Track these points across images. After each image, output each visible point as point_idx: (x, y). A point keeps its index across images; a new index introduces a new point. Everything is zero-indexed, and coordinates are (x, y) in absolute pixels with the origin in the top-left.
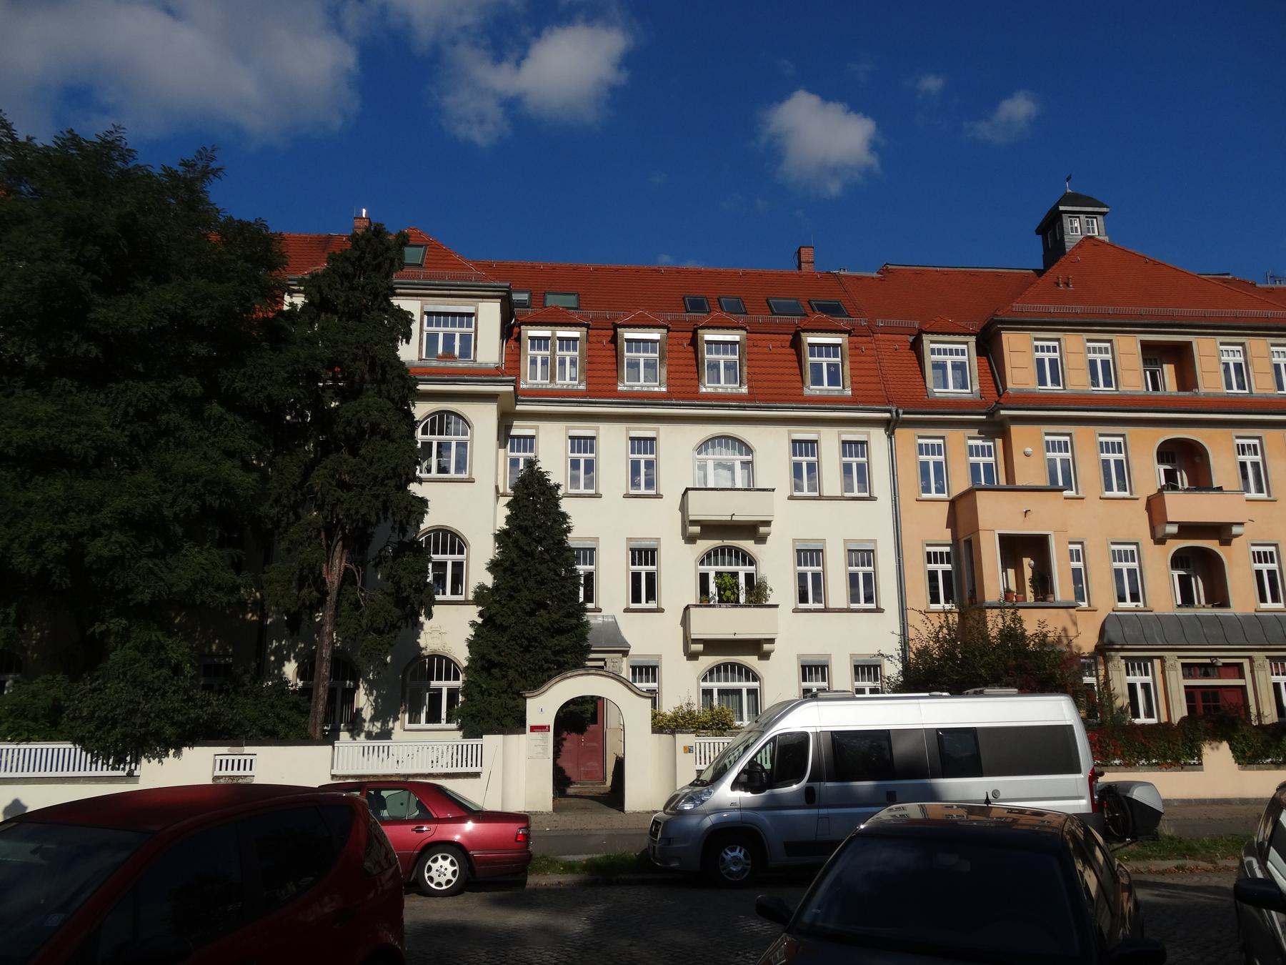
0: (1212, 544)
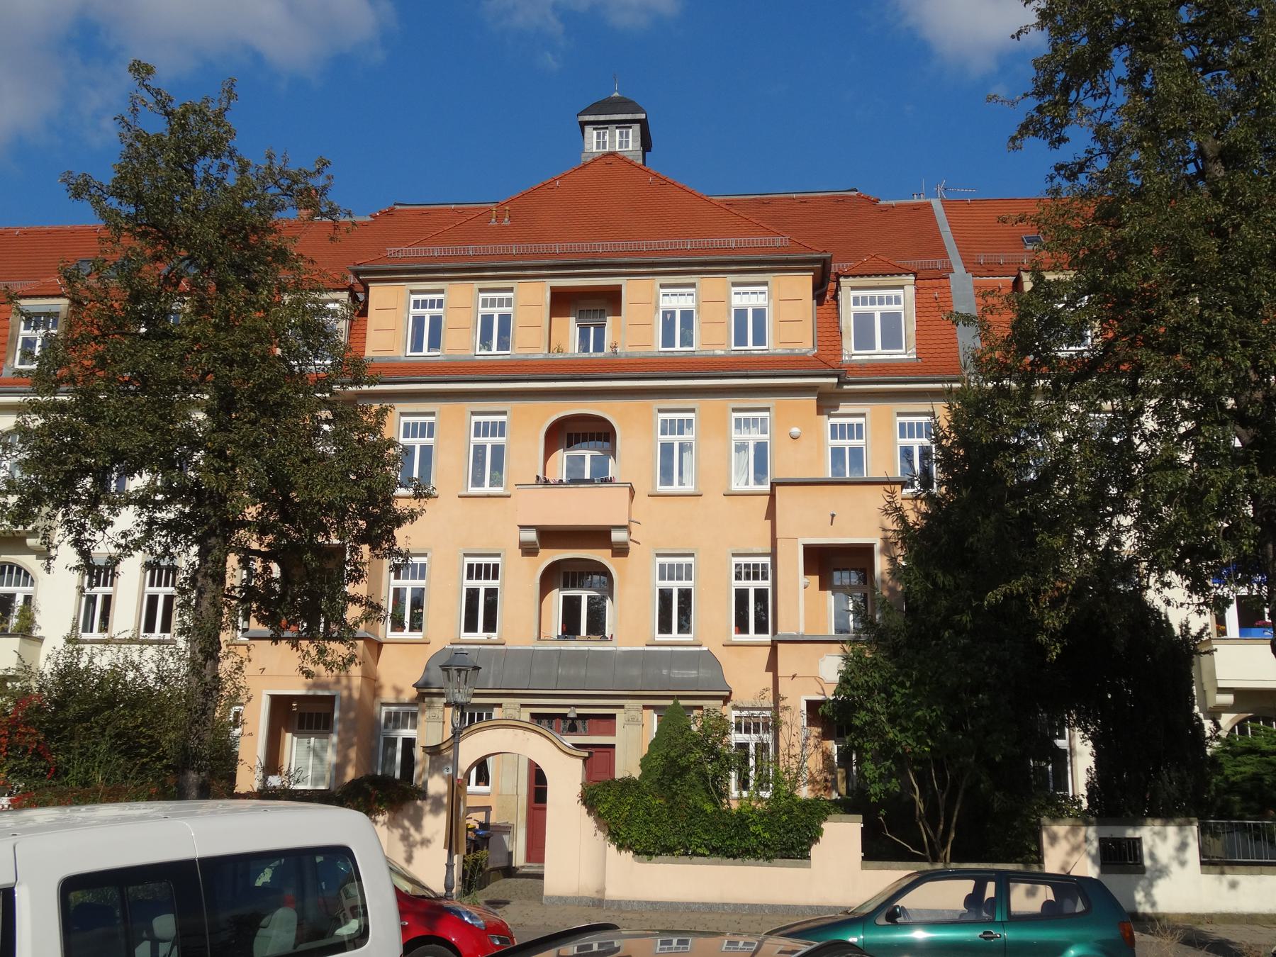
0: (601, 555)
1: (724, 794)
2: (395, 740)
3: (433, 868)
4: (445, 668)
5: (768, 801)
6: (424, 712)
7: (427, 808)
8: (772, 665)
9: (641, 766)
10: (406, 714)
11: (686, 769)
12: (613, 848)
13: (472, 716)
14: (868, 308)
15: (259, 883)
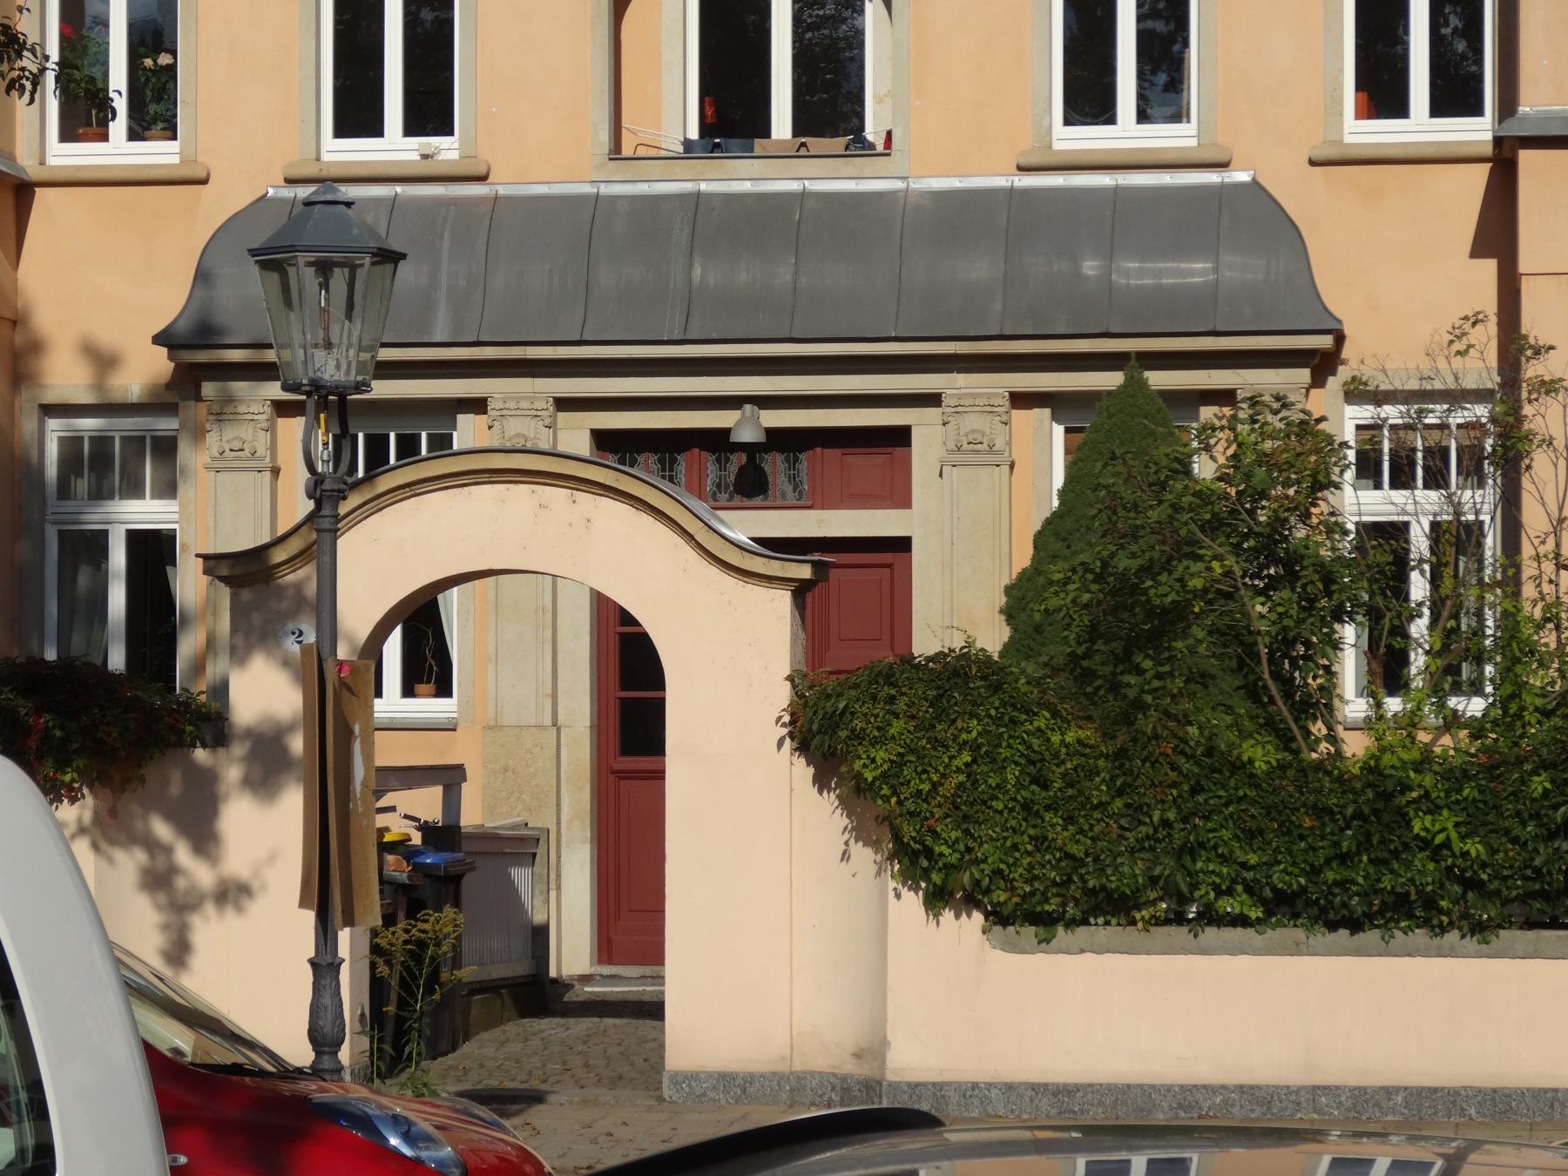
1: (1321, 704)
2: (97, 544)
3: (265, 977)
4: (272, 260)
5: (1477, 728)
6: (199, 435)
7: (233, 773)
8: (1497, 233)
9: (1009, 613)
10: (135, 444)
11: (1173, 619)
12: (912, 902)
13: (375, 443)
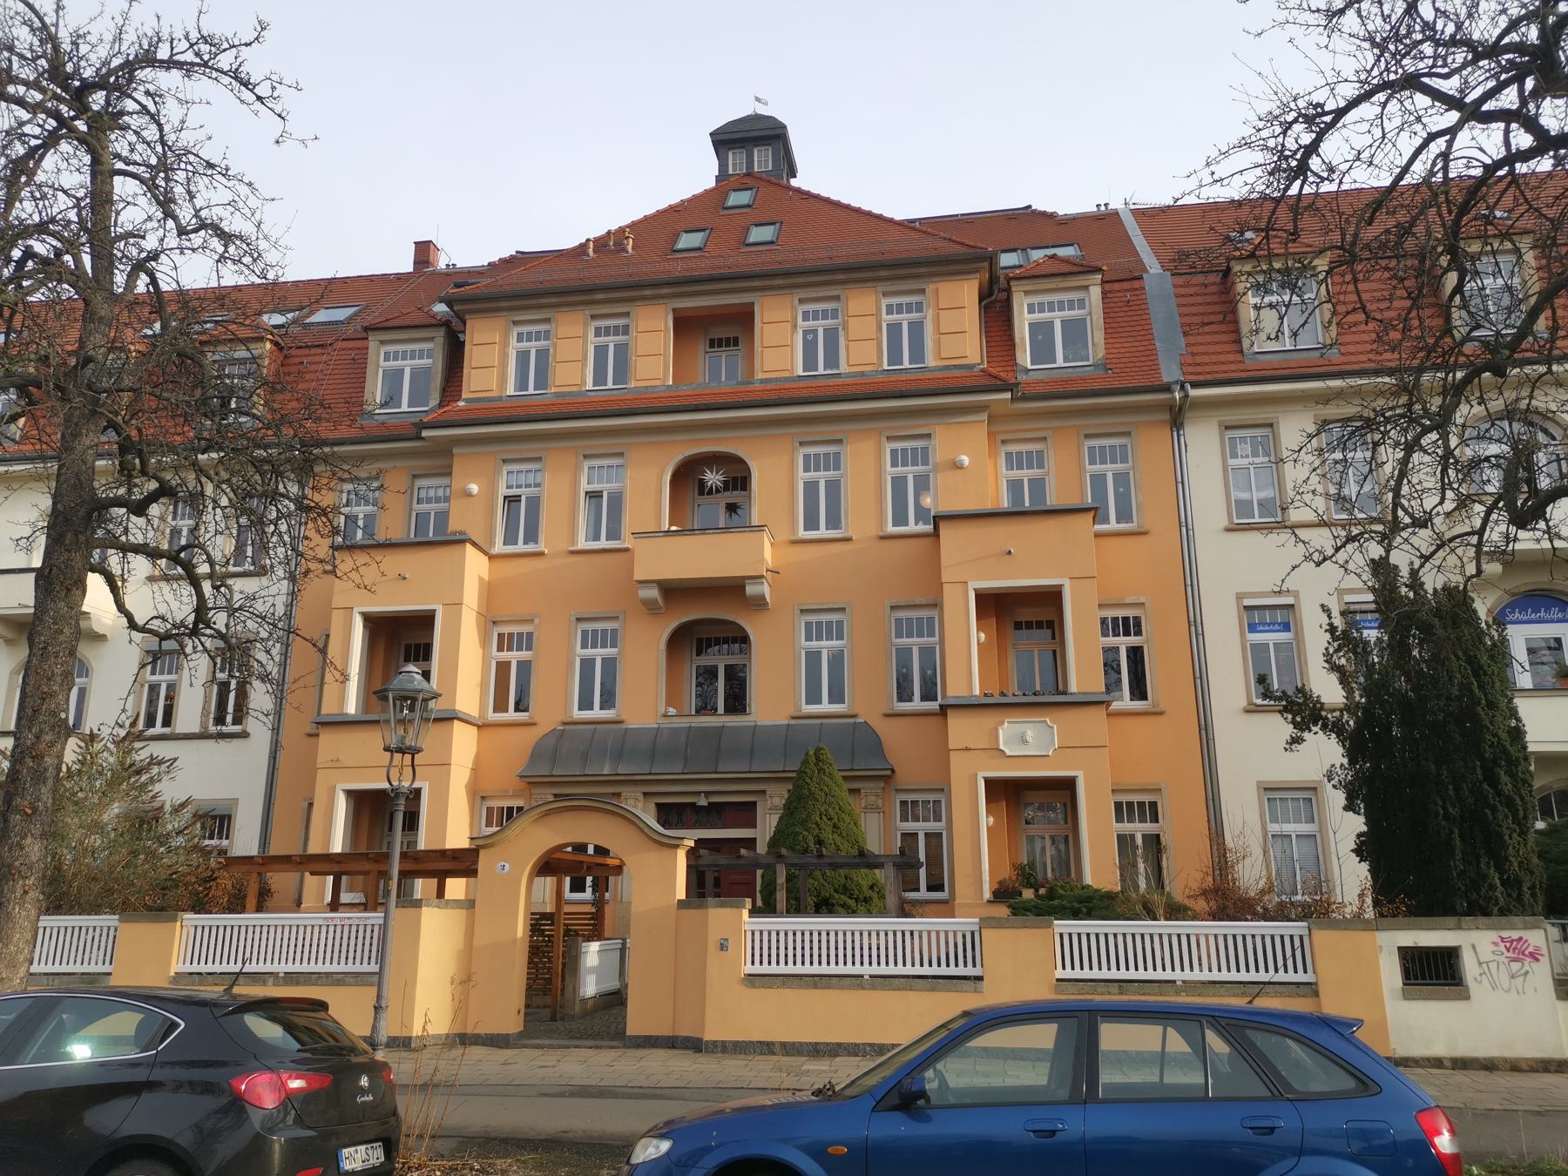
14: (1046, 315)
15: (665, 1146)
